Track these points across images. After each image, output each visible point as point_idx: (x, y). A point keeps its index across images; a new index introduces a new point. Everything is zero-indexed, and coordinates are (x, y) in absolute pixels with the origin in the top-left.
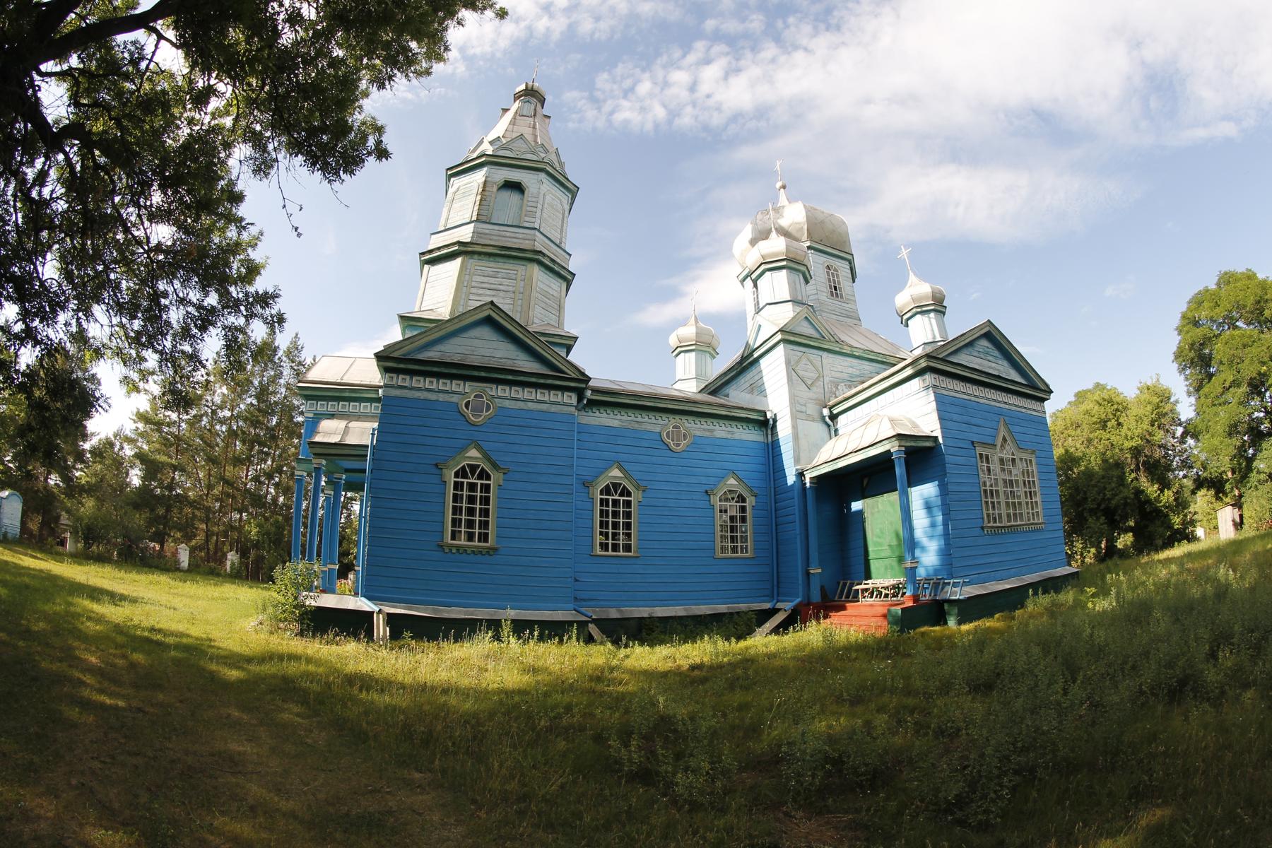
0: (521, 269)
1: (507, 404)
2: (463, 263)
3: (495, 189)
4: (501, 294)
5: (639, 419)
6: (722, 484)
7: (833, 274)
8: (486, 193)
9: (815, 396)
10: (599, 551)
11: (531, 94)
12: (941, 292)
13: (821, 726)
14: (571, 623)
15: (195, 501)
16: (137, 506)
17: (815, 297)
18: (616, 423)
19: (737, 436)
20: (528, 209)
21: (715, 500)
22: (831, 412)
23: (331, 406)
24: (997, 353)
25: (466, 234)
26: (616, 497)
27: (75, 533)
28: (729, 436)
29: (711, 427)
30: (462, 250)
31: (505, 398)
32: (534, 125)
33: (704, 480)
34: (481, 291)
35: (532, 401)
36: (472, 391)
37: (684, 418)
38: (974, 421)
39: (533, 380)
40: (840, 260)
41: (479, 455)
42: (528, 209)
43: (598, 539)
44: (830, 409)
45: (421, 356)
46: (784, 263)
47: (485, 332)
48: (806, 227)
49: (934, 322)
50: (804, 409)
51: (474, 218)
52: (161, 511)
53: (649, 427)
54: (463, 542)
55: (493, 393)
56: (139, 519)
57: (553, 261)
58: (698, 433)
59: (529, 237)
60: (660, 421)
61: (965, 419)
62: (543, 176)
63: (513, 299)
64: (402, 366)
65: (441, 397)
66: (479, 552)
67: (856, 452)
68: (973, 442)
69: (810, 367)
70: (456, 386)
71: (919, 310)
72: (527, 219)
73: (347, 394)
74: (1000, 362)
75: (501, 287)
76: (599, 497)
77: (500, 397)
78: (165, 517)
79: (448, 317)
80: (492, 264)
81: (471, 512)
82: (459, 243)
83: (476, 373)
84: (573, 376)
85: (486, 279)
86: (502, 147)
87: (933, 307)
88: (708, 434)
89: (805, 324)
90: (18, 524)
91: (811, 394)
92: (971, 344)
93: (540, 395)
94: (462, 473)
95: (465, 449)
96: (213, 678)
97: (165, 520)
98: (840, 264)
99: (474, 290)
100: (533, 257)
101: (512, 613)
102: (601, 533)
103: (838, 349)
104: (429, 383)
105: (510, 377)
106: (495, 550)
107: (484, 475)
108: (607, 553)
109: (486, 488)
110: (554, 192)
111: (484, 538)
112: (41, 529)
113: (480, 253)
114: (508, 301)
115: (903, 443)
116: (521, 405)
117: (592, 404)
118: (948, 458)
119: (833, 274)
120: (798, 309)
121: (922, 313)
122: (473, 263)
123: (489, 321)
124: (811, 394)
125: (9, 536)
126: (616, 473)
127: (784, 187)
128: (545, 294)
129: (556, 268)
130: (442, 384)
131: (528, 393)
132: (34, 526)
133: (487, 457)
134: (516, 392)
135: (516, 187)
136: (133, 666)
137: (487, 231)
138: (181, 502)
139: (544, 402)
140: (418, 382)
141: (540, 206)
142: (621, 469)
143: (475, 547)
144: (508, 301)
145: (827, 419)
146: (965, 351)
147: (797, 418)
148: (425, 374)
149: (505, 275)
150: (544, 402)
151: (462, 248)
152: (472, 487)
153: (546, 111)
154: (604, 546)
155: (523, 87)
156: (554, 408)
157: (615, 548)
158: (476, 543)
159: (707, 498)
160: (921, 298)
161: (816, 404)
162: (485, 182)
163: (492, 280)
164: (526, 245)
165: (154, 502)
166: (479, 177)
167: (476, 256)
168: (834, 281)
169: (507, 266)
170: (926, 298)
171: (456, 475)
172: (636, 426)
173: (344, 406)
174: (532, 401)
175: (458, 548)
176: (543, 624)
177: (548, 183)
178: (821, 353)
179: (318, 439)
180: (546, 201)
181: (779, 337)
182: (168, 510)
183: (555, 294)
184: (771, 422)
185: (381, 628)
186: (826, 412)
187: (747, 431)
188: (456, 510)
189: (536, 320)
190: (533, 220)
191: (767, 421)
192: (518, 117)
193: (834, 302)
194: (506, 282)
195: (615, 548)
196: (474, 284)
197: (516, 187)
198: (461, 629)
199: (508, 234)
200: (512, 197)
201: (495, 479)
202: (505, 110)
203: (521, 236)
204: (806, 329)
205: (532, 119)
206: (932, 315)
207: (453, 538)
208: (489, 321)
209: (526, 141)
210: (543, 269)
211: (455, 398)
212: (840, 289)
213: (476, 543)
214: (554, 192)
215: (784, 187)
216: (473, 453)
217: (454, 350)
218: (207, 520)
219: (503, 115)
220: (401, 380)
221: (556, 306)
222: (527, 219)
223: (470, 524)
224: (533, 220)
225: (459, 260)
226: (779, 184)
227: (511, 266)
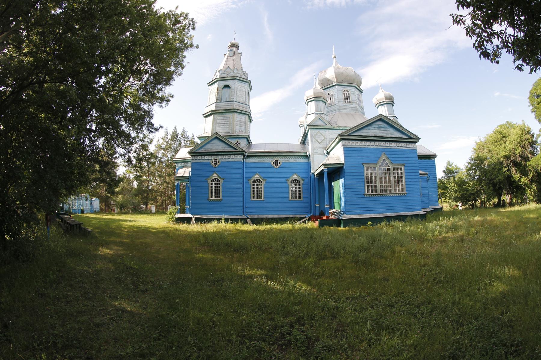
0: (230, 115)
1: (223, 161)
2: (213, 117)
3: (221, 89)
4: (225, 125)
5: (264, 159)
6: (291, 177)
7: (346, 94)
8: (218, 92)
9: (322, 146)
10: (252, 199)
11: (233, 46)
12: (390, 95)
13: (201, 255)
14: (238, 219)
15: (156, 190)
16: (136, 195)
17: (338, 104)
18: (257, 161)
19: (297, 161)
20: (232, 94)
21: (289, 182)
22: (327, 151)
23: (183, 164)
24: (387, 126)
25: (213, 108)
26: (257, 183)
27: (117, 207)
28: (295, 161)
29: (288, 159)
30: (213, 113)
31: (223, 159)
32: (234, 60)
33: (285, 176)
34: (219, 125)
35: (230, 159)
36: (214, 158)
37: (279, 157)
38: (365, 155)
39: (229, 153)
40: (350, 87)
41: (216, 175)
42: (232, 94)
43: (252, 195)
44: (327, 150)
45: (200, 151)
46: (313, 99)
47: (216, 141)
48: (335, 77)
49: (386, 108)
50: (317, 151)
51: (216, 102)
52: (146, 195)
53: (267, 161)
54: (214, 198)
55: (219, 158)
56: (138, 199)
57: (240, 110)
58: (284, 162)
59: (232, 104)
60: (271, 159)
61: (360, 155)
62: (236, 80)
63: (229, 126)
64: (195, 154)
65: (206, 161)
66: (217, 201)
67: (319, 168)
68: (362, 164)
69: (321, 136)
70: (209, 157)
71: (380, 104)
72: (232, 98)
73: (186, 161)
74: (388, 130)
75: (225, 123)
76: (252, 183)
77: (221, 159)
78: (147, 197)
79: (211, 135)
80: (222, 116)
81: (215, 190)
82: (211, 111)
83: (214, 154)
84: (240, 151)
85: (220, 121)
86: (223, 73)
87: (385, 103)
88: (287, 162)
89: (319, 121)
90: (99, 207)
91: (321, 146)
92: (370, 125)
93: (232, 157)
94: (212, 181)
95: (213, 174)
96: (150, 231)
97: (147, 198)
98: (349, 89)
99: (217, 125)
100: (233, 111)
101: (226, 216)
102: (253, 194)
103: (332, 128)
104: (202, 158)
105: (223, 153)
106: (222, 200)
107: (218, 180)
108: (254, 199)
109: (219, 184)
110: (241, 85)
111: (219, 197)
112: (105, 207)
113: (218, 113)
114: (228, 127)
115: (326, 166)
116: (227, 160)
117: (248, 156)
118: (346, 170)
119: (346, 94)
120: (317, 115)
121: (382, 105)
122: (217, 116)
123: (216, 138)
124: (321, 146)
125: (97, 211)
126: (257, 176)
127: (335, 57)
128: (240, 121)
129: (242, 112)
130: (206, 158)
131: (228, 157)
132: (103, 207)
133: (218, 176)
134: (225, 157)
135: (227, 87)
136: (134, 230)
137: (219, 105)
138: (152, 191)
139: (233, 159)
140: (199, 158)
141: (235, 92)
142: (259, 175)
143: (214, 199)
144: (228, 127)
145: (326, 154)
146: (366, 128)
147: (314, 155)
148: (201, 155)
149: (226, 118)
150: (233, 159)
151: (213, 112)
152: (215, 184)
153: (239, 51)
154: (254, 197)
155: (230, 44)
156: (236, 160)
157: (257, 198)
158: (217, 198)
159: (286, 182)
160: (380, 100)
161: (323, 149)
162: (218, 88)
163: (222, 121)
164: (231, 107)
165: (142, 193)
166: (216, 86)
167: (217, 114)
168: (347, 96)
169: (226, 115)
170: (383, 99)
171: (211, 181)
172: (263, 161)
173: (186, 164)
174: (230, 159)
175: (212, 200)
176: (231, 219)
177: (239, 83)
178: (326, 130)
179: (177, 175)
180: (238, 89)
181: (308, 127)
182: (148, 194)
183: (244, 120)
184: (309, 156)
185: (193, 221)
186: (325, 152)
187: (302, 159)
188: (212, 190)
189: (237, 131)
190: (233, 98)
191: (307, 156)
192: (228, 58)
193: (346, 105)
194: (226, 120)
195: (257, 198)
196: (217, 123)
197: (227, 87)
198: (209, 220)
199: (226, 105)
200: (226, 90)
201: (221, 181)
202: (225, 55)
203: (230, 104)
204: (320, 123)
205: (233, 57)
206: (386, 105)
207: (211, 197)
208: (216, 138)
209: (230, 69)
210: (238, 114)
211: (209, 161)
212: (350, 99)
213: (217, 198)
214: (241, 85)
215: (335, 57)
216: (215, 175)
217: (209, 148)
218: (161, 196)
219: (224, 56)
220: (195, 158)
221: (244, 124)
222: (232, 98)
223: (215, 194)
224: (233, 98)
225: (212, 116)
226: (333, 56)
227: (228, 115)
